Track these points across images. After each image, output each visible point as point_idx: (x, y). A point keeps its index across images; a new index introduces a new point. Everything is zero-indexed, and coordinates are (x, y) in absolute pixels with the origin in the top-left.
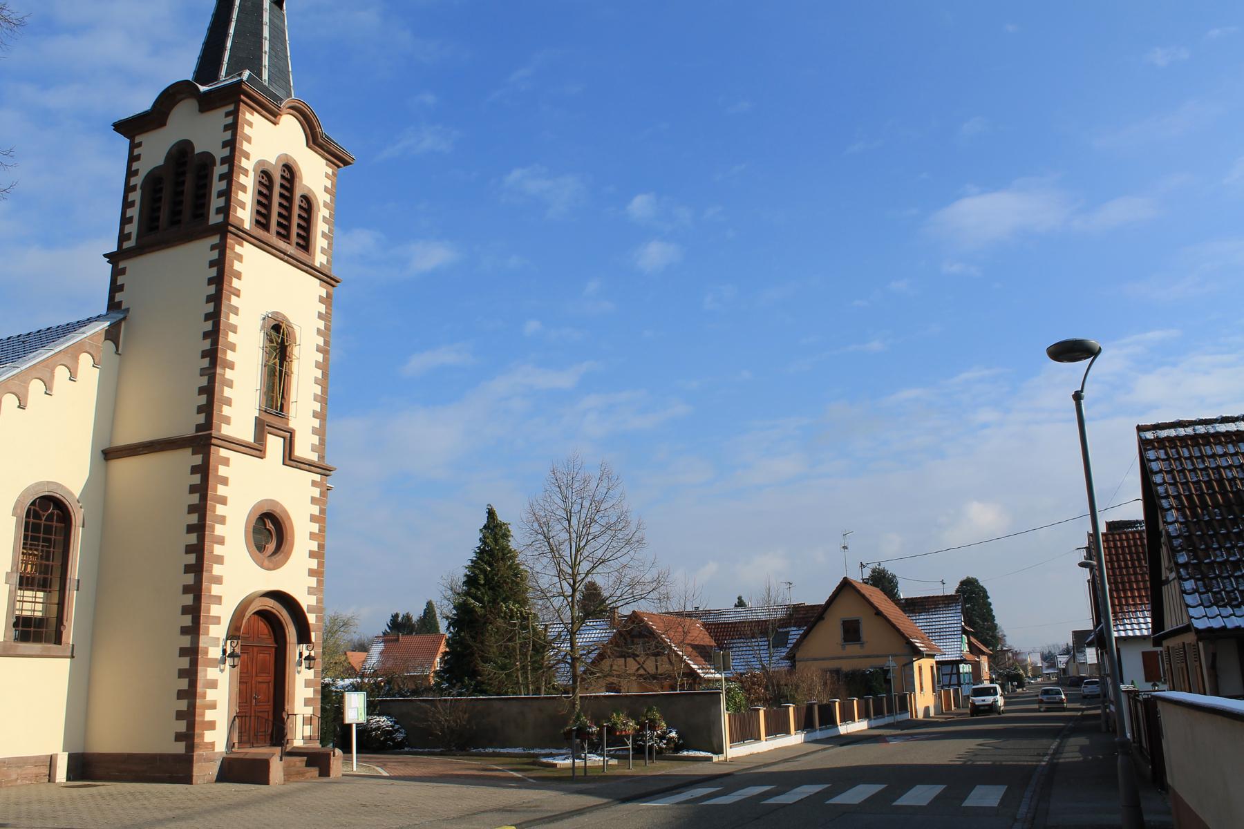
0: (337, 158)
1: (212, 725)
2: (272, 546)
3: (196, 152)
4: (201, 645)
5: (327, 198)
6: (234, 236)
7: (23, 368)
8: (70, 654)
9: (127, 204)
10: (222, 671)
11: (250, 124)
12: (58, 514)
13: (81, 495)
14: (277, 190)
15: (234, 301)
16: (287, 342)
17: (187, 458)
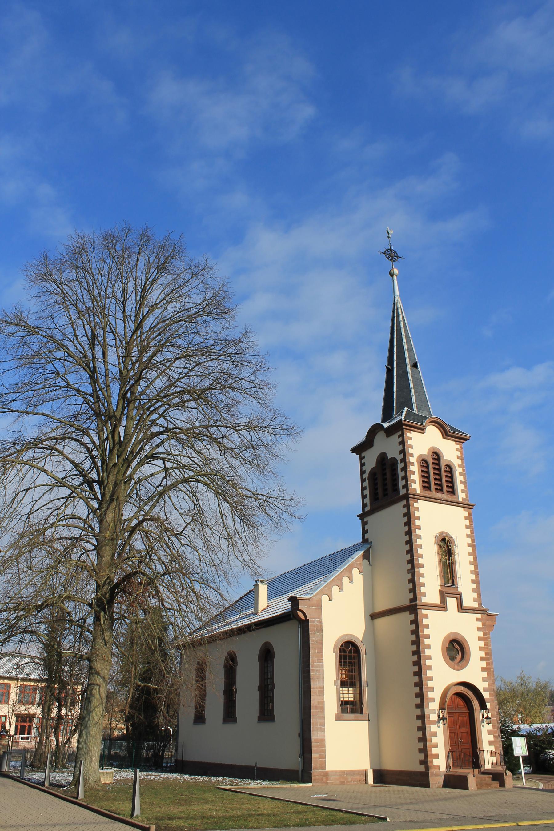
0: (460, 438)
1: (437, 756)
2: (459, 657)
3: (389, 458)
5: (460, 461)
7: (328, 582)
8: (367, 719)
9: (363, 489)
10: (439, 727)
11: (411, 439)
12: (354, 649)
13: (363, 638)
14: (431, 466)
15: (418, 532)
16: (450, 546)
17: (407, 617)
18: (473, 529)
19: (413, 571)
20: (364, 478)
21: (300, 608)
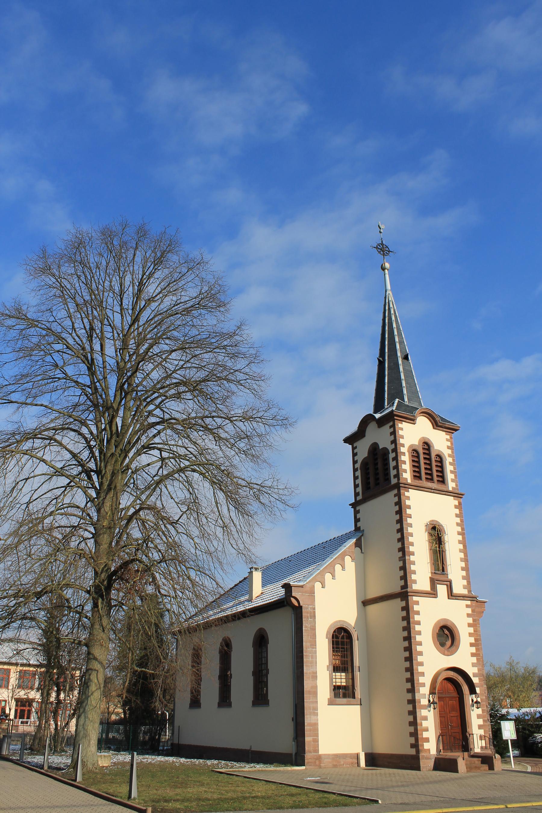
0: (450, 429)
1: (427, 740)
2: (449, 643)
4: (416, 698)
5: (450, 451)
6: (404, 488)
7: (321, 569)
8: (359, 703)
9: (355, 478)
10: (429, 711)
11: (402, 429)
12: (346, 635)
14: (422, 456)
15: (409, 520)
17: (398, 603)
18: (463, 517)
19: (404, 558)
20: (356, 467)
21: (293, 594)
